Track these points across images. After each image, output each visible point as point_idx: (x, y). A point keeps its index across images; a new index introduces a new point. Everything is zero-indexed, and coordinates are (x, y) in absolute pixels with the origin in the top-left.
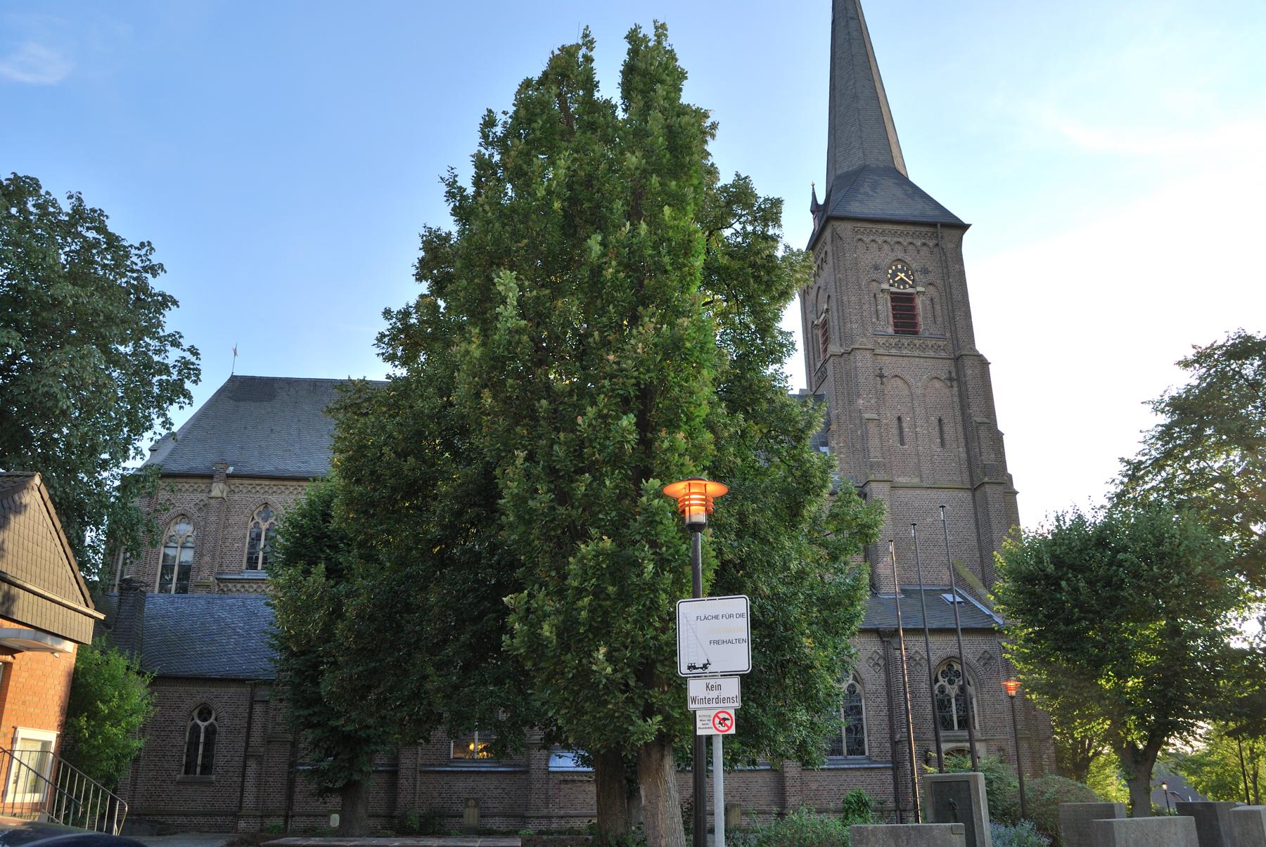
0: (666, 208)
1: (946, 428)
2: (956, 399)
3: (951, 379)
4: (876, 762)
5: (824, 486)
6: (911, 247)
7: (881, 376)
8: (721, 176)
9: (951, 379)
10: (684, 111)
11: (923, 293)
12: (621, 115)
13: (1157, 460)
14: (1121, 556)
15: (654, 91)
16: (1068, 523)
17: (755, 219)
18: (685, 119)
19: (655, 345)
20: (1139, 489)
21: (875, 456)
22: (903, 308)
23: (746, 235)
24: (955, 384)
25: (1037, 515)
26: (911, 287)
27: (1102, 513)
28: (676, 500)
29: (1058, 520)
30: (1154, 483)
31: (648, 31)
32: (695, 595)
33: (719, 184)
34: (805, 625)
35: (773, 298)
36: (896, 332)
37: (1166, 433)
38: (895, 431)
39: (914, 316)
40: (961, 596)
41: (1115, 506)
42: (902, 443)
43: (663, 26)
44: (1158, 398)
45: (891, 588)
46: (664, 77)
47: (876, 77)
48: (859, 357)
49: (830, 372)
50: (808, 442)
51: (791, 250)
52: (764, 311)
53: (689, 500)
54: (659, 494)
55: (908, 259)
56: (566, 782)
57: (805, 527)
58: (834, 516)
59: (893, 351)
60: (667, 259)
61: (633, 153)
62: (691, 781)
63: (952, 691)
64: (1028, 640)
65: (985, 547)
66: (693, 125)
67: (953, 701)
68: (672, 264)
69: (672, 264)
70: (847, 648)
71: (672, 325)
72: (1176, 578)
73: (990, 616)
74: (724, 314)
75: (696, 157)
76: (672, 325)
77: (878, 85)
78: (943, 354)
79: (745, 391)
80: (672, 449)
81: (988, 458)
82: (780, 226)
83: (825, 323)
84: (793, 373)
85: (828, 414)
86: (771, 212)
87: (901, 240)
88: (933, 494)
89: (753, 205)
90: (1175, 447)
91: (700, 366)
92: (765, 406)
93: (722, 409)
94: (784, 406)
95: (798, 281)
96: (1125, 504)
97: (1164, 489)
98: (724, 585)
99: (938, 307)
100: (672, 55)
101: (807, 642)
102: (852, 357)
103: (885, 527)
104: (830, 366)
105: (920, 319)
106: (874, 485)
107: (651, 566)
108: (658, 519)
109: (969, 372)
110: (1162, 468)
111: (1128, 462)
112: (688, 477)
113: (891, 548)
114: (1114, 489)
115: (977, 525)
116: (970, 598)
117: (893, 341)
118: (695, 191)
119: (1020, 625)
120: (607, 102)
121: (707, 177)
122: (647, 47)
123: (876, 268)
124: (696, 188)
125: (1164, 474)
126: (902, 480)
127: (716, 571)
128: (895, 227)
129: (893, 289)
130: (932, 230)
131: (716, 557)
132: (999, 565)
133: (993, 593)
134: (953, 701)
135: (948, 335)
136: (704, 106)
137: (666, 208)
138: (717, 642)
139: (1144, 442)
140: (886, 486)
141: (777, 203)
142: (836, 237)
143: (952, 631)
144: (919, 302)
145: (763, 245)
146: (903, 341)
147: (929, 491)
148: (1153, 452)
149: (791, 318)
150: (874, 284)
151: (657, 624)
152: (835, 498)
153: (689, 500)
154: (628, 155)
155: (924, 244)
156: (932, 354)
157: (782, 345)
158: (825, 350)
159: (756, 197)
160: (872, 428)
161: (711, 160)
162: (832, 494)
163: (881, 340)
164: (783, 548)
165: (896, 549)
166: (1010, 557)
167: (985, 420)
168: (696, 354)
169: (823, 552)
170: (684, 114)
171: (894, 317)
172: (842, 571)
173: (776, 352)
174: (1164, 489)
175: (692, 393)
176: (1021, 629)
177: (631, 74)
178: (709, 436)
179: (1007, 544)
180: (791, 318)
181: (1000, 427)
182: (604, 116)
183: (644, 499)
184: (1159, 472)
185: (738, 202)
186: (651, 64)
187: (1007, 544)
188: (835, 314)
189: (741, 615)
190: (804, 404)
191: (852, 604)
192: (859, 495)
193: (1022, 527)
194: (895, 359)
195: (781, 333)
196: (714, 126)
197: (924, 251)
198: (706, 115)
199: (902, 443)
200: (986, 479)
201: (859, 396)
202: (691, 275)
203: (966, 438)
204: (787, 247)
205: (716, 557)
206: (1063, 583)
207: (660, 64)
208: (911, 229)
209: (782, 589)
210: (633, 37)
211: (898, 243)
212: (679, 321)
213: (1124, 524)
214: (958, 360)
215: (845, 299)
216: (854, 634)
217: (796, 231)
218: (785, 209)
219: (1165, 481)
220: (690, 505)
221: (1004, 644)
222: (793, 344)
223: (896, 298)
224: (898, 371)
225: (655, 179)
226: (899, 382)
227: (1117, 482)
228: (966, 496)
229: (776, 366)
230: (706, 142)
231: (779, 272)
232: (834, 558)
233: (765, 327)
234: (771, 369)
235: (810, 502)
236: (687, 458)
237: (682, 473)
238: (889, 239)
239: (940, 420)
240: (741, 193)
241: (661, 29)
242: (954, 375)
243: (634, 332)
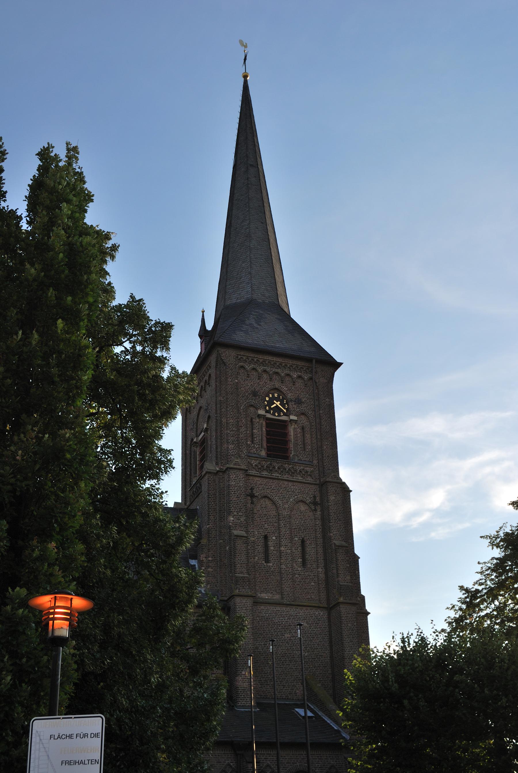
0: (60, 321)
1: (308, 550)
2: (318, 522)
3: (315, 503)
5: (189, 601)
6: (287, 378)
7: (252, 496)
8: (117, 296)
9: (315, 503)
10: (89, 231)
11: (295, 421)
12: (24, 226)
13: (491, 590)
14: (457, 678)
15: (60, 208)
16: (412, 644)
17: (145, 340)
18: (87, 239)
19: (35, 453)
20: (475, 615)
21: (241, 572)
23: (134, 353)
24: (319, 508)
25: (383, 638)
26: (285, 414)
27: (442, 638)
28: (41, 611)
29: (403, 641)
30: (488, 611)
31: (60, 151)
32: (51, 712)
33: (115, 303)
34: (161, 739)
35: (155, 416)
36: (268, 455)
37: (499, 566)
38: (260, 548)
39: (286, 442)
40: (312, 711)
41: (454, 630)
42: (267, 561)
43: (75, 149)
44: (493, 533)
45: (248, 701)
46: (71, 196)
47: (268, 222)
48: (233, 476)
49: (204, 488)
50: (178, 557)
51: (177, 371)
52: (146, 428)
53: (54, 613)
54: (24, 604)
55: (284, 389)
57: (168, 641)
58: (196, 630)
59: (265, 473)
60: (54, 371)
61: (32, 265)
64: (371, 756)
65: (337, 662)
66: (94, 246)
68: (59, 376)
69: (59, 376)
70: (201, 763)
71: (54, 435)
72: (504, 700)
73: (338, 732)
74: (107, 427)
75: (94, 276)
76: (54, 435)
77: (269, 228)
78: (309, 480)
79: (123, 499)
80: (42, 558)
81: (344, 579)
82: (168, 349)
83: (204, 441)
84: (170, 489)
85: (199, 531)
86: (162, 334)
87: (279, 371)
88: (292, 611)
89: (144, 327)
90: (507, 579)
91: (77, 479)
92: (139, 519)
93: (97, 520)
94: (157, 520)
95: (180, 402)
96: (463, 629)
97: (496, 617)
98: (78, 707)
99: (308, 436)
100: (80, 178)
101: (162, 757)
102: (226, 476)
103: (246, 639)
104: (205, 482)
106: (238, 600)
107: (9, 678)
108: (20, 629)
109: (332, 498)
110: (495, 597)
111: (467, 591)
112: (55, 589)
113: (250, 663)
114: (453, 614)
115: (331, 642)
116: (320, 713)
117: (265, 464)
118: (90, 309)
119: (364, 741)
120: (13, 213)
121: (103, 297)
122: (57, 166)
123: (255, 394)
124: (91, 305)
125: (497, 603)
126: (265, 596)
127: (75, 684)
128: (275, 359)
129: (269, 416)
130: (307, 364)
131: (77, 670)
132: (348, 682)
133: (342, 710)
135: (315, 462)
136: (104, 227)
137: (60, 321)
138: (69, 763)
139: (481, 573)
140: (248, 602)
141: (167, 327)
142: (220, 362)
143: (301, 746)
144: (291, 430)
145: (151, 365)
146: (275, 464)
147: (288, 609)
148: (488, 583)
149: (172, 437)
150: (252, 409)
151: (10, 739)
152: (200, 611)
153: (54, 613)
154: (28, 266)
155: (299, 377)
156: (300, 478)
157: (160, 462)
158: (202, 467)
159: (148, 319)
160: (240, 545)
161: (108, 279)
162: (199, 606)
163: (254, 463)
164: (145, 660)
165: (254, 663)
166: (358, 674)
167: (344, 543)
168: (76, 465)
169: (184, 666)
170: (88, 234)
171: (268, 442)
172: (200, 685)
173: (158, 466)
174: (496, 617)
175: (67, 504)
176: (366, 745)
177: (37, 187)
178: (80, 547)
179: (357, 662)
180: (172, 437)
181: (357, 551)
182: (8, 225)
183: (9, 608)
184: (493, 601)
185: (130, 322)
186: (60, 183)
187: (357, 662)
188: (214, 434)
189: (96, 735)
190: (177, 520)
191: (209, 720)
192: (223, 609)
193: (372, 646)
194: (265, 481)
195: (161, 450)
196: (115, 248)
198: (107, 237)
199: (267, 561)
200: (341, 600)
201: (229, 513)
202: (77, 388)
203: (325, 560)
204: (173, 368)
205: (77, 670)
206: (406, 702)
207: (68, 184)
208: (290, 362)
209: (141, 702)
210: (45, 154)
211: (277, 373)
212: (62, 432)
213: (460, 647)
214: (322, 485)
215: (224, 420)
216: (208, 749)
217: (183, 355)
218: (174, 333)
219: (497, 609)
220: (54, 619)
221: (350, 759)
222: (171, 461)
223: (270, 423)
225: (51, 292)
226: (268, 502)
227: (457, 608)
228: (322, 614)
229: (153, 482)
230: (105, 262)
231: (163, 392)
232: (194, 672)
233: (148, 437)
234: (148, 484)
235: (175, 617)
236: (57, 568)
237: (49, 582)
238: (268, 369)
239: (303, 542)
240: (134, 313)
241: (73, 152)
242: (318, 499)
243: (16, 438)
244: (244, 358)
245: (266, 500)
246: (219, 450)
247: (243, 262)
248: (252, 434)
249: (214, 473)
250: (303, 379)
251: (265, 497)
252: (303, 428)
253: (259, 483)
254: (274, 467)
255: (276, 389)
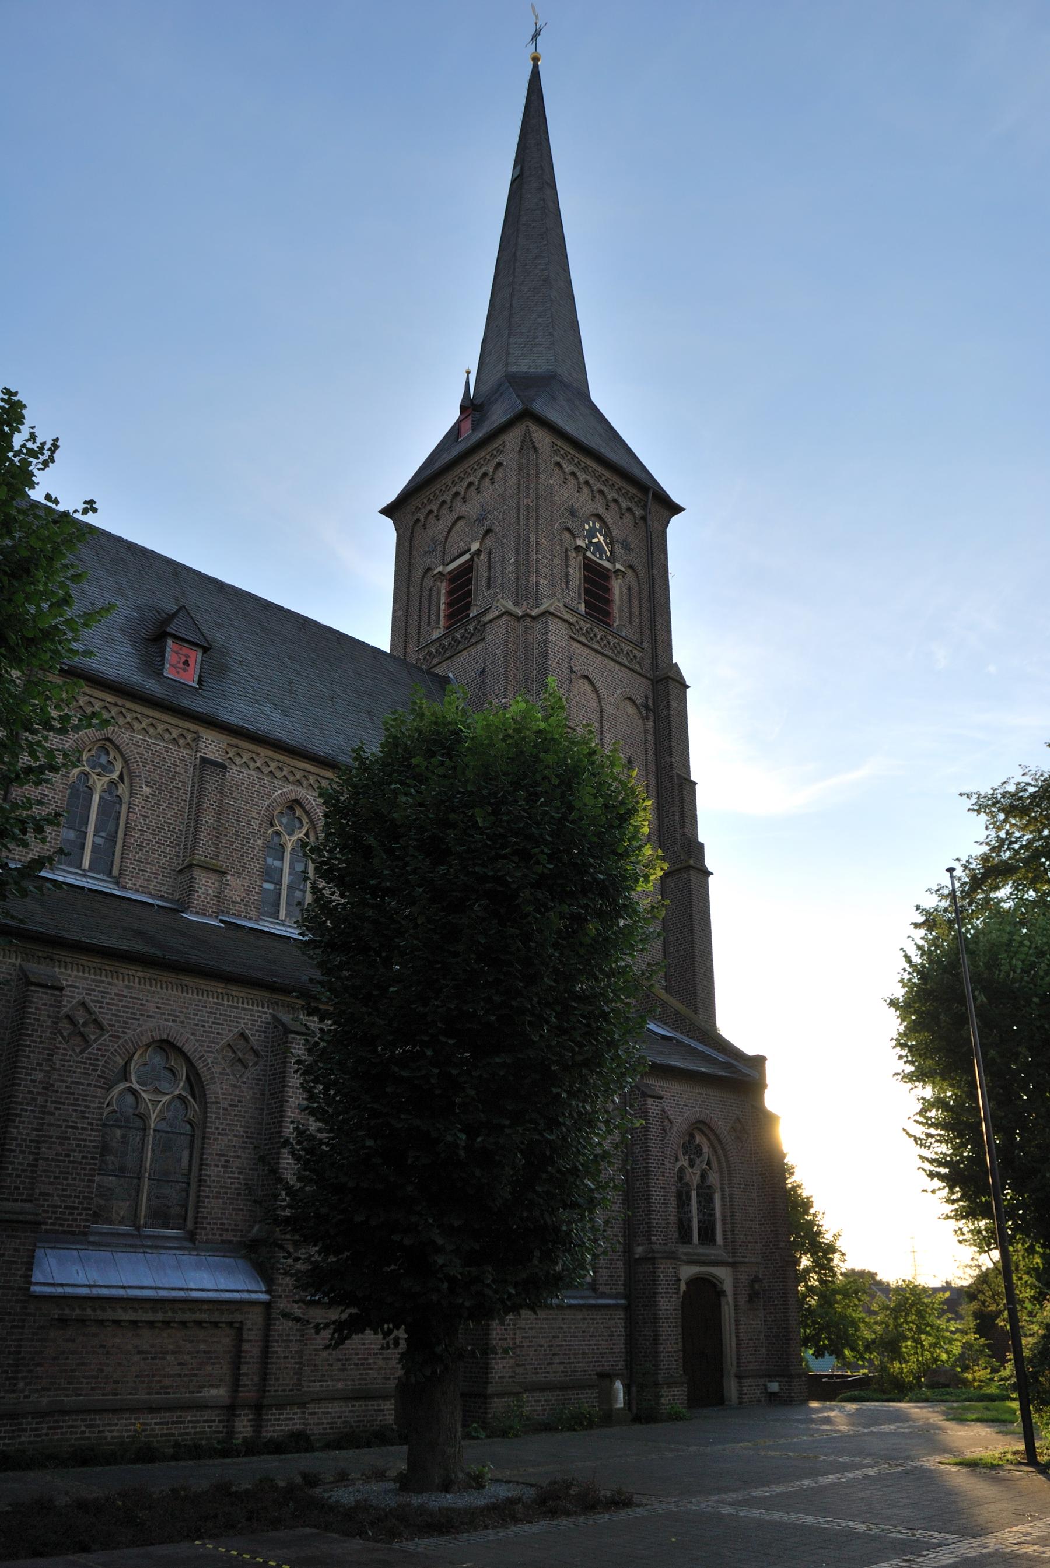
4: (603, 1295)
9: (647, 707)
22: (596, 581)
39: (608, 602)
56: (63, 1322)
62: (621, 1323)
63: (693, 1178)
67: (694, 1194)
102: (538, 626)
105: (615, 610)
123: (573, 513)
128: (600, 469)
134: (694, 1194)
142: (528, 445)
146: (596, 630)
150: (567, 535)
155: (629, 509)
197: (628, 518)
211: (601, 492)
215: (533, 537)
224: (589, 671)
226: (587, 687)
244: (562, 452)
245: (586, 682)
246: (522, 582)
247: (540, 316)
248: (567, 574)
249: (516, 617)
250: (634, 514)
251: (586, 677)
252: (629, 589)
253: (578, 651)
254: (595, 636)
255: (598, 517)
